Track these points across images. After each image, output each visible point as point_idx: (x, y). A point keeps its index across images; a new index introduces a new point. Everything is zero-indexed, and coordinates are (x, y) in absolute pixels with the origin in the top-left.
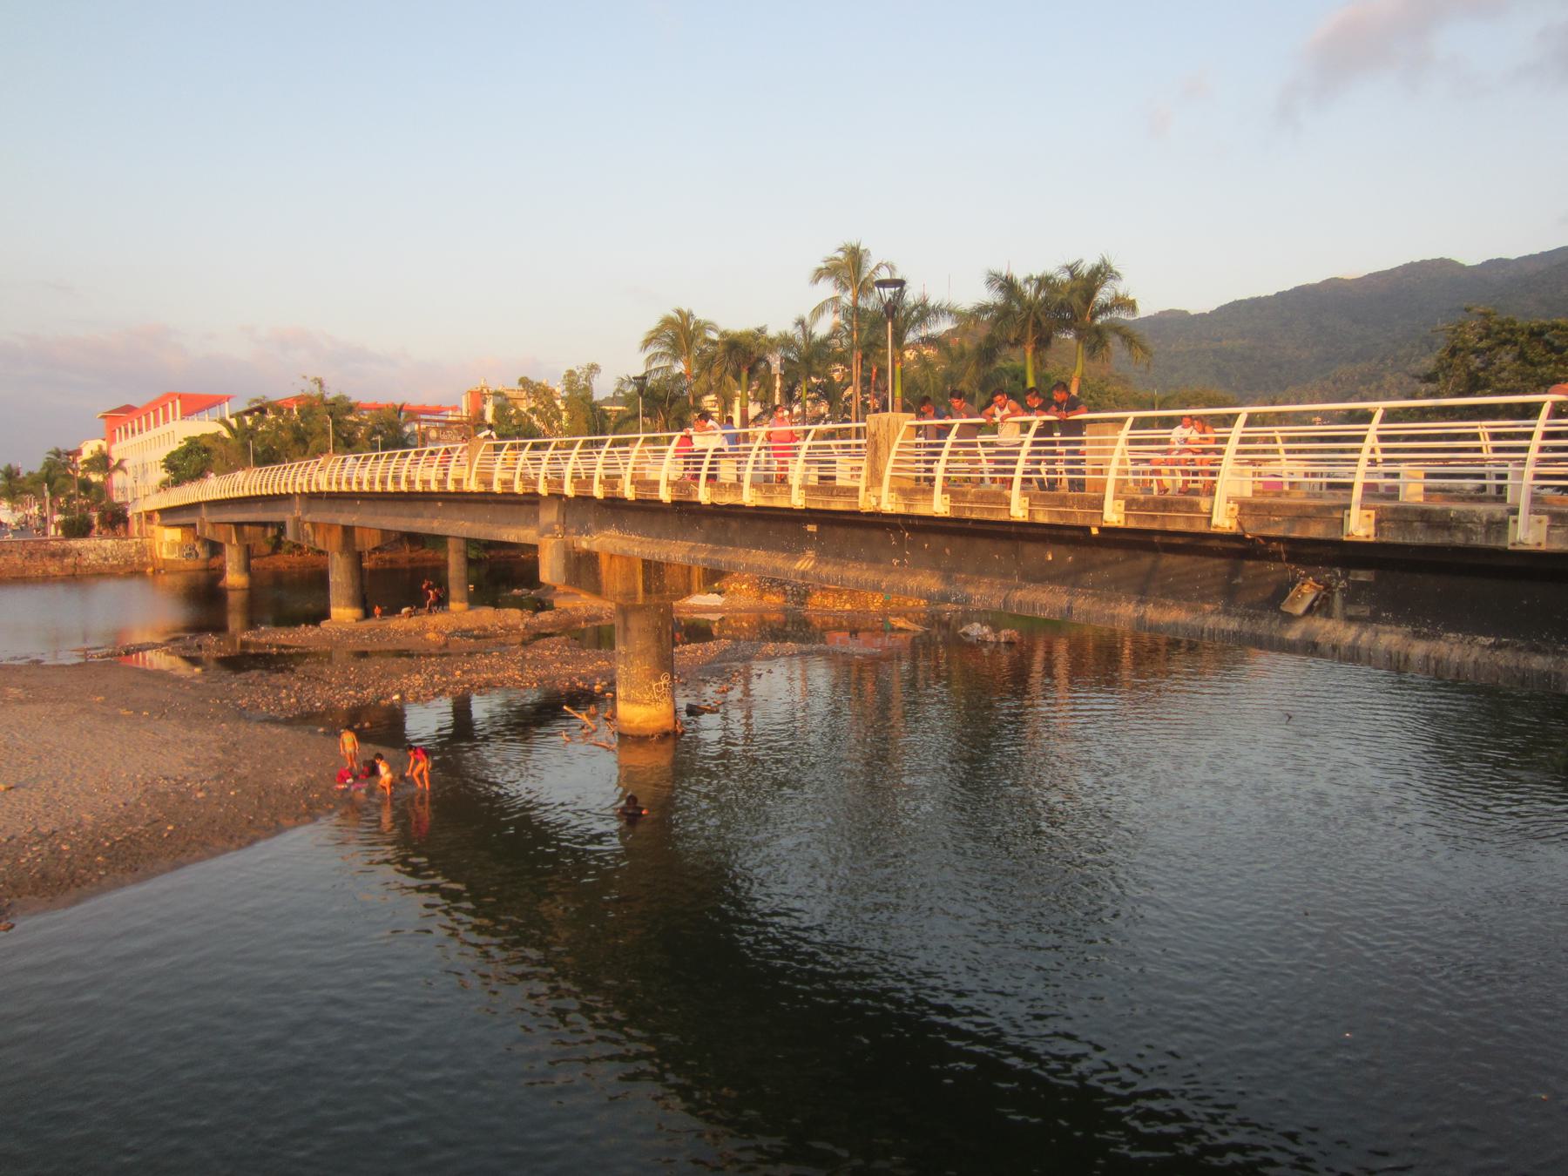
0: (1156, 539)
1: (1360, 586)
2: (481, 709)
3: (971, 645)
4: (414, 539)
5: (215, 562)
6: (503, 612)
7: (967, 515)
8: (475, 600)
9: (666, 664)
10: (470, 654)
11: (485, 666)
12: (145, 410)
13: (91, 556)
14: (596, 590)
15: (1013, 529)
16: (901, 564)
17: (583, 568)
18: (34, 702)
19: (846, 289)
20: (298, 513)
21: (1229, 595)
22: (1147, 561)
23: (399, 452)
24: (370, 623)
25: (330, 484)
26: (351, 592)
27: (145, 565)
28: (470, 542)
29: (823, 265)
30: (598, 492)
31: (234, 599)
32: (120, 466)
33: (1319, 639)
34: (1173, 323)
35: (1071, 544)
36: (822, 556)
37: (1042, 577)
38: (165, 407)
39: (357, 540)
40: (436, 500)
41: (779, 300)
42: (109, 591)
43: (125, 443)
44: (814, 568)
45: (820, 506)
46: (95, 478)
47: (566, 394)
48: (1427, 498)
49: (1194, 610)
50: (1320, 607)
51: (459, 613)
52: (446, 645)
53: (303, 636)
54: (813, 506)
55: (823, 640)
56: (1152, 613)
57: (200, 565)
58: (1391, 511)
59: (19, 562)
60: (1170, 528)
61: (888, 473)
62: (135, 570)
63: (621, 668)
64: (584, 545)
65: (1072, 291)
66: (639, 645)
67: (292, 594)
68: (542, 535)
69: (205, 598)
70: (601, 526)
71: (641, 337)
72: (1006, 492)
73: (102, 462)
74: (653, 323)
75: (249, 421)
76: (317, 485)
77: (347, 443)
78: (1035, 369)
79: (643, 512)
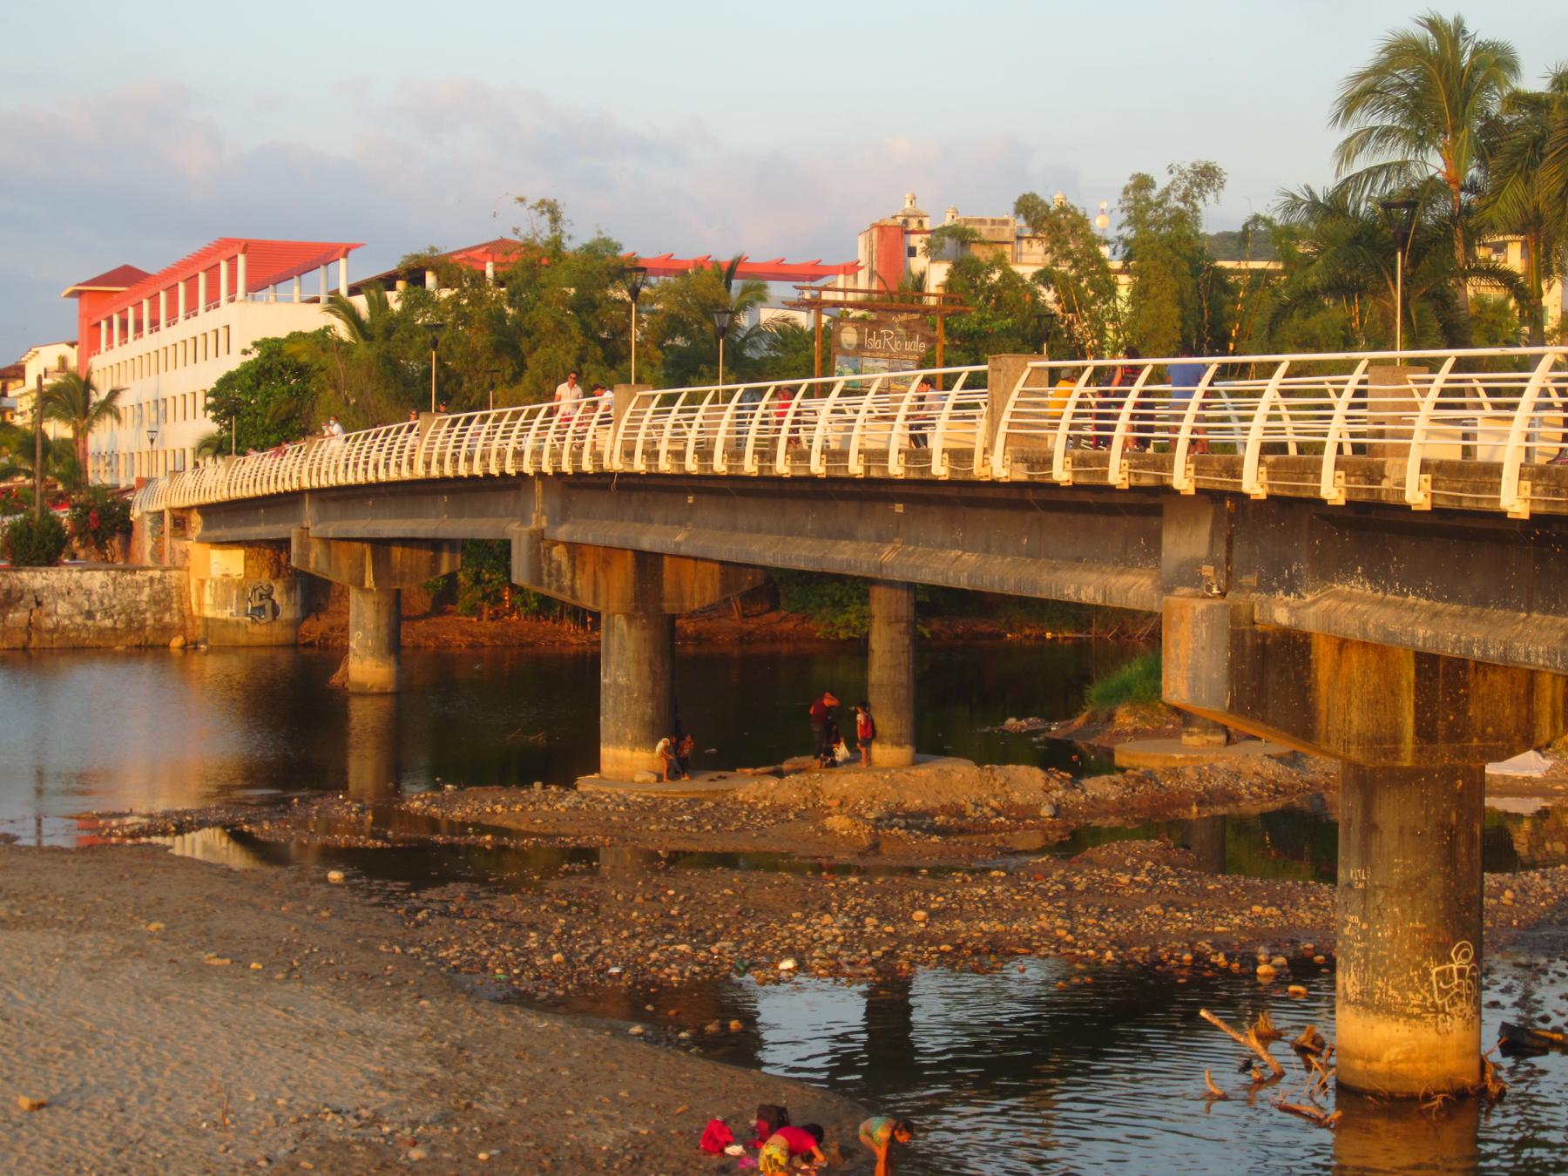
2: (937, 1008)
4: (773, 586)
5: (316, 628)
8: (930, 742)
9: (1462, 920)
12: (168, 280)
13: (63, 608)
14: (1302, 723)
17: (1272, 674)
18: (30, 925)
20: (538, 519)
25: (629, 454)
26: (649, 710)
27: (166, 630)
28: (933, 602)
30: (1332, 488)
31: (363, 716)
32: (108, 406)
39: (668, 588)
40: (891, 499)
42: (89, 683)
46: (57, 429)
47: (1128, 233)
52: (875, 847)
53: (532, 810)
57: (280, 633)
62: (148, 643)
63: (1351, 924)
64: (1282, 617)
68: (1167, 589)
69: (292, 708)
70: (1328, 569)
71: (1332, 92)
73: (73, 398)
76: (597, 456)
77: (603, 361)
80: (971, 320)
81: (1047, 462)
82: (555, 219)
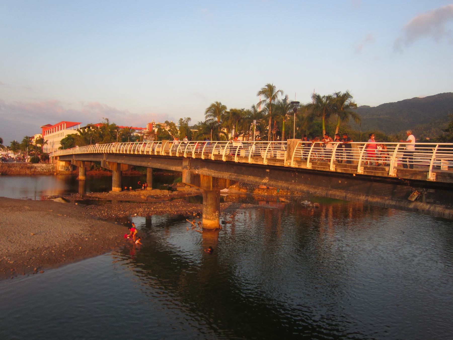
0: (372, 178)
1: (431, 193)
2: (154, 220)
3: (304, 207)
5: (74, 172)
6: (163, 191)
7: (317, 169)
8: (154, 187)
9: (217, 208)
10: (155, 203)
11: (160, 207)
12: (55, 126)
15: (329, 173)
16: (295, 182)
17: (195, 179)
18: (33, 210)
19: (268, 98)
20: (104, 159)
21: (393, 195)
22: (369, 184)
23: (131, 143)
24: (124, 192)
25: (116, 151)
27: (54, 172)
28: (155, 170)
29: (261, 90)
30: (203, 157)
31: (81, 183)
32: (46, 143)
33: (419, 208)
34: (366, 109)
35: (346, 178)
36: (270, 179)
37: (337, 187)
38: (61, 126)
39: (121, 168)
41: (245, 98)
43: (48, 135)
44: (268, 182)
45: (272, 164)
46: (39, 145)
47: (180, 126)
48: (449, 169)
49: (382, 198)
50: (419, 199)
51: (148, 191)
52: (147, 200)
54: (270, 164)
55: (258, 204)
56: (370, 199)
57: (70, 173)
58: (440, 174)
59: (19, 169)
60: (377, 175)
61: (293, 156)
62: (51, 174)
64: (197, 172)
65: (337, 101)
66: (210, 202)
67: (100, 182)
68: (183, 169)
69: (71, 182)
70: (202, 167)
72: (329, 163)
73: (41, 141)
74: (209, 106)
75: (86, 130)
76: (112, 151)
78: (325, 124)
79: (217, 164)
80: (161, 135)
81: (169, 153)
82: (108, 121)
